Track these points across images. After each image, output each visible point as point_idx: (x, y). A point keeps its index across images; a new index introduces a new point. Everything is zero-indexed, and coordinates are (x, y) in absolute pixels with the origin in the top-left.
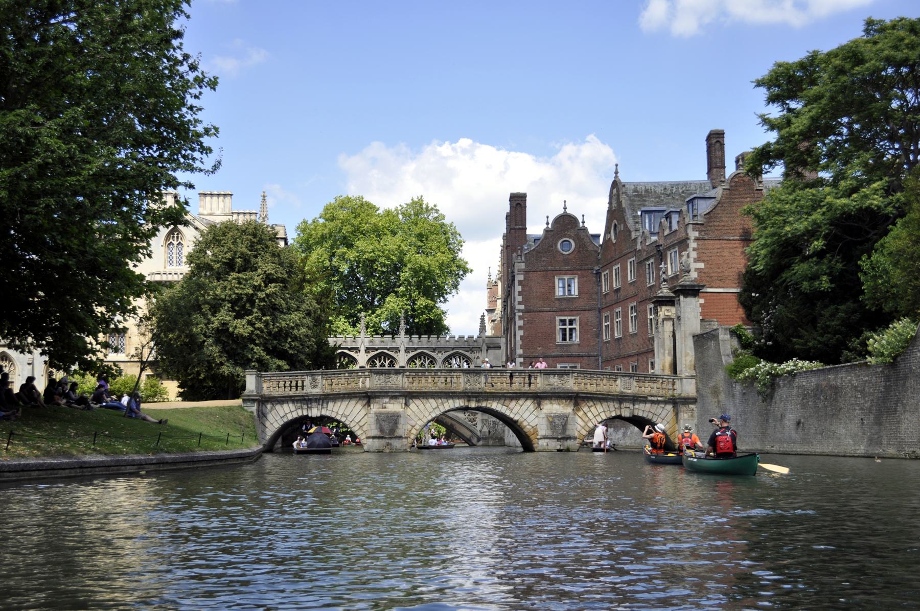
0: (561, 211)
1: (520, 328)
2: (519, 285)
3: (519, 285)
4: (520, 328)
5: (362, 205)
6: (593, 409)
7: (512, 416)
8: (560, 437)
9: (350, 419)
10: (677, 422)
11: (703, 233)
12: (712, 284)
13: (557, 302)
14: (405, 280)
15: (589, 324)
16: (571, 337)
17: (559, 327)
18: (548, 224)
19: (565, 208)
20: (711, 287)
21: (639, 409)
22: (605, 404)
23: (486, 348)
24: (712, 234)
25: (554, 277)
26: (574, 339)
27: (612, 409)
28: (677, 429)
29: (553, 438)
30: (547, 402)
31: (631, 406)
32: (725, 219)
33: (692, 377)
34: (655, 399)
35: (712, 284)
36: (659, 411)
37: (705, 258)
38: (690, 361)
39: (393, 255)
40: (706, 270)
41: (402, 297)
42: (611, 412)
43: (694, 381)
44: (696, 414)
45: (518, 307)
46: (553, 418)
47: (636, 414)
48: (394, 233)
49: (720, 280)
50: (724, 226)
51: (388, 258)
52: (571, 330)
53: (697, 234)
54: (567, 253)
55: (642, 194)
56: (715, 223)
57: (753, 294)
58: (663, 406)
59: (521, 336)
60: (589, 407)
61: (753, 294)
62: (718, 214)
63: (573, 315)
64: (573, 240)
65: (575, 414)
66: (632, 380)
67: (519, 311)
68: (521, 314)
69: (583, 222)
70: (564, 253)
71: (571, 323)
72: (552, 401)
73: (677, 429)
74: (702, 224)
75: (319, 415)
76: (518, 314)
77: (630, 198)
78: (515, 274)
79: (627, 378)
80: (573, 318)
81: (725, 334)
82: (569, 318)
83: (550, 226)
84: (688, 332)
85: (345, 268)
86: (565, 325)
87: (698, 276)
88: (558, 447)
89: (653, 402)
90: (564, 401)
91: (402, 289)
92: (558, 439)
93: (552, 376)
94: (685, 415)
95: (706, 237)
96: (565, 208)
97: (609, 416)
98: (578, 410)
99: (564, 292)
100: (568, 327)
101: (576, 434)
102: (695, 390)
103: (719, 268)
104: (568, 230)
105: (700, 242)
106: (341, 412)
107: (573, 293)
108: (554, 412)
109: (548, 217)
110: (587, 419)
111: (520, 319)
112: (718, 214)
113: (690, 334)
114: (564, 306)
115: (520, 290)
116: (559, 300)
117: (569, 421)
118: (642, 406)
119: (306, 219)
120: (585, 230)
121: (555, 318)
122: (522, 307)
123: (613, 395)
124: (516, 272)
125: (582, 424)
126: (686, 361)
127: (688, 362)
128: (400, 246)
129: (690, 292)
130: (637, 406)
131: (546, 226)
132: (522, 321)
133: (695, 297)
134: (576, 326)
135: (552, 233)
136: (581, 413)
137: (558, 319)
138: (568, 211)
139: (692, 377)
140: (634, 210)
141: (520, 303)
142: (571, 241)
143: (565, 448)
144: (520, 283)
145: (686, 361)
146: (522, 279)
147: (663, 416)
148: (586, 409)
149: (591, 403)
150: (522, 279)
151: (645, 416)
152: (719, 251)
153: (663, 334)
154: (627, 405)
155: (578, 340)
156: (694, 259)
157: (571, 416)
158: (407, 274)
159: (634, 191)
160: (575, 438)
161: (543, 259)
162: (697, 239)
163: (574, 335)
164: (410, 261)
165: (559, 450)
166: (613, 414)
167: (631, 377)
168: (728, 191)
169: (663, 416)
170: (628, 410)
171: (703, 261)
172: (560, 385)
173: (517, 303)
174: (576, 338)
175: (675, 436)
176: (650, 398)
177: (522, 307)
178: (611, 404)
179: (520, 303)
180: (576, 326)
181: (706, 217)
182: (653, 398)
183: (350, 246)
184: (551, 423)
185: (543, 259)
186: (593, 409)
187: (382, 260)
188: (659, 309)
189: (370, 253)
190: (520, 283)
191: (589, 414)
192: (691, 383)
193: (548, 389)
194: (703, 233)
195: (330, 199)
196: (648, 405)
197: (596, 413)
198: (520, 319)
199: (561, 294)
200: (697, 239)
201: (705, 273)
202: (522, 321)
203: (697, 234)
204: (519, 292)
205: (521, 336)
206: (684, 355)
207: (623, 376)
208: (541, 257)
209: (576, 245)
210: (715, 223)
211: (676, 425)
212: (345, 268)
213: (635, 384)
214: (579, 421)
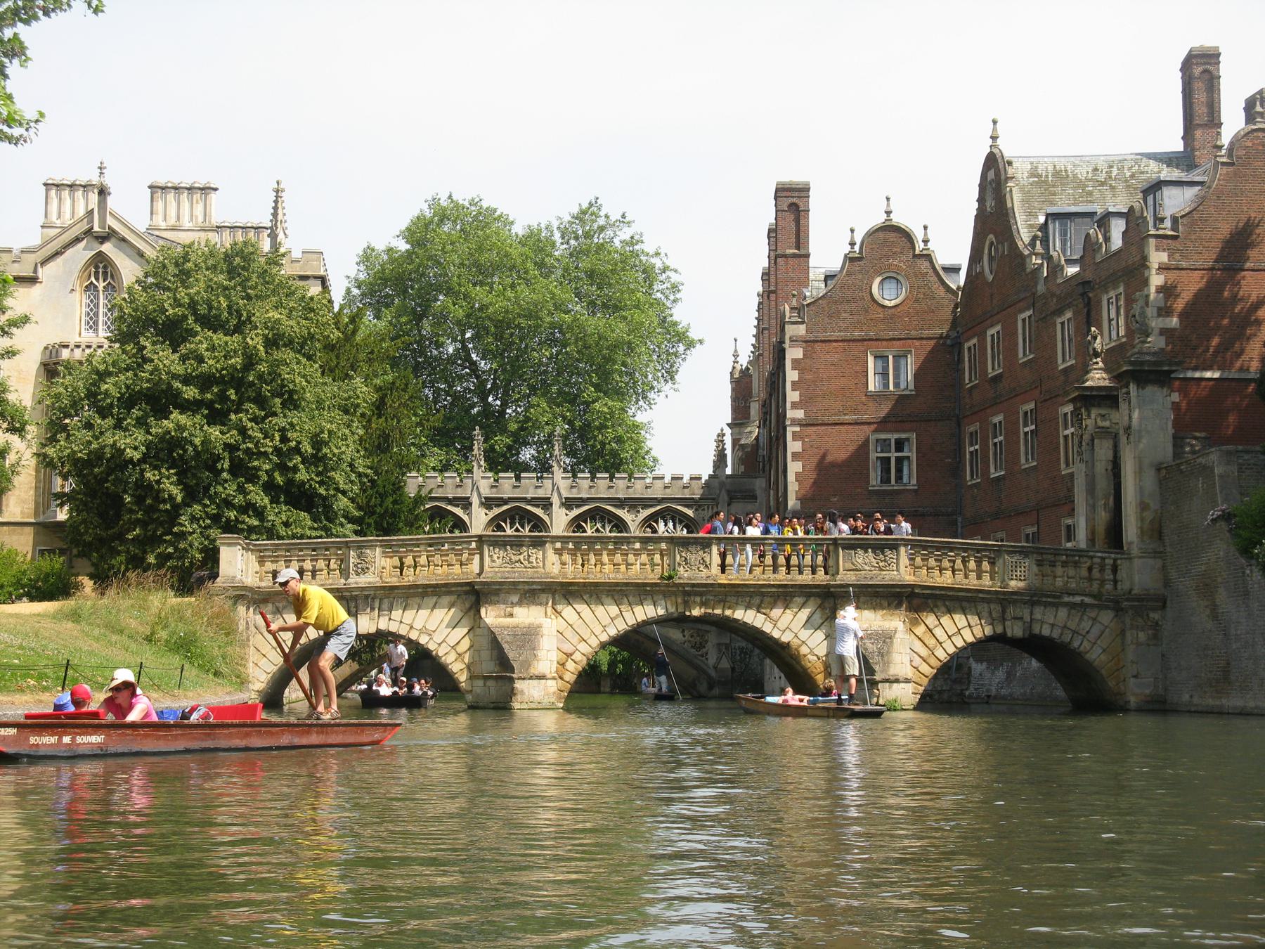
0: (880, 219)
1: (796, 456)
3: (794, 368)
4: (796, 456)
7: (776, 634)
9: (438, 638)
11: (1177, 256)
16: (899, 478)
18: (852, 244)
19: (888, 213)
23: (726, 498)
24: (1196, 257)
47: (1036, 630)
54: (893, 303)
59: (797, 474)
63: (904, 431)
67: (795, 422)
69: (926, 241)
70: (887, 303)
71: (900, 445)
75: (373, 630)
80: (904, 436)
82: (896, 436)
83: (857, 248)
95: (1184, 264)
96: (888, 213)
106: (418, 625)
109: (852, 231)
111: (794, 440)
120: (928, 257)
122: (799, 414)
124: (787, 341)
131: (848, 248)
134: (910, 452)
138: (897, 219)
147: (1092, 636)
155: (914, 481)
162: (1162, 268)
169: (1092, 636)
170: (1020, 623)
177: (799, 414)
179: (795, 406)
190: (796, 362)
191: (939, 632)
194: (1177, 256)
198: (794, 440)
204: (793, 383)
205: (797, 474)
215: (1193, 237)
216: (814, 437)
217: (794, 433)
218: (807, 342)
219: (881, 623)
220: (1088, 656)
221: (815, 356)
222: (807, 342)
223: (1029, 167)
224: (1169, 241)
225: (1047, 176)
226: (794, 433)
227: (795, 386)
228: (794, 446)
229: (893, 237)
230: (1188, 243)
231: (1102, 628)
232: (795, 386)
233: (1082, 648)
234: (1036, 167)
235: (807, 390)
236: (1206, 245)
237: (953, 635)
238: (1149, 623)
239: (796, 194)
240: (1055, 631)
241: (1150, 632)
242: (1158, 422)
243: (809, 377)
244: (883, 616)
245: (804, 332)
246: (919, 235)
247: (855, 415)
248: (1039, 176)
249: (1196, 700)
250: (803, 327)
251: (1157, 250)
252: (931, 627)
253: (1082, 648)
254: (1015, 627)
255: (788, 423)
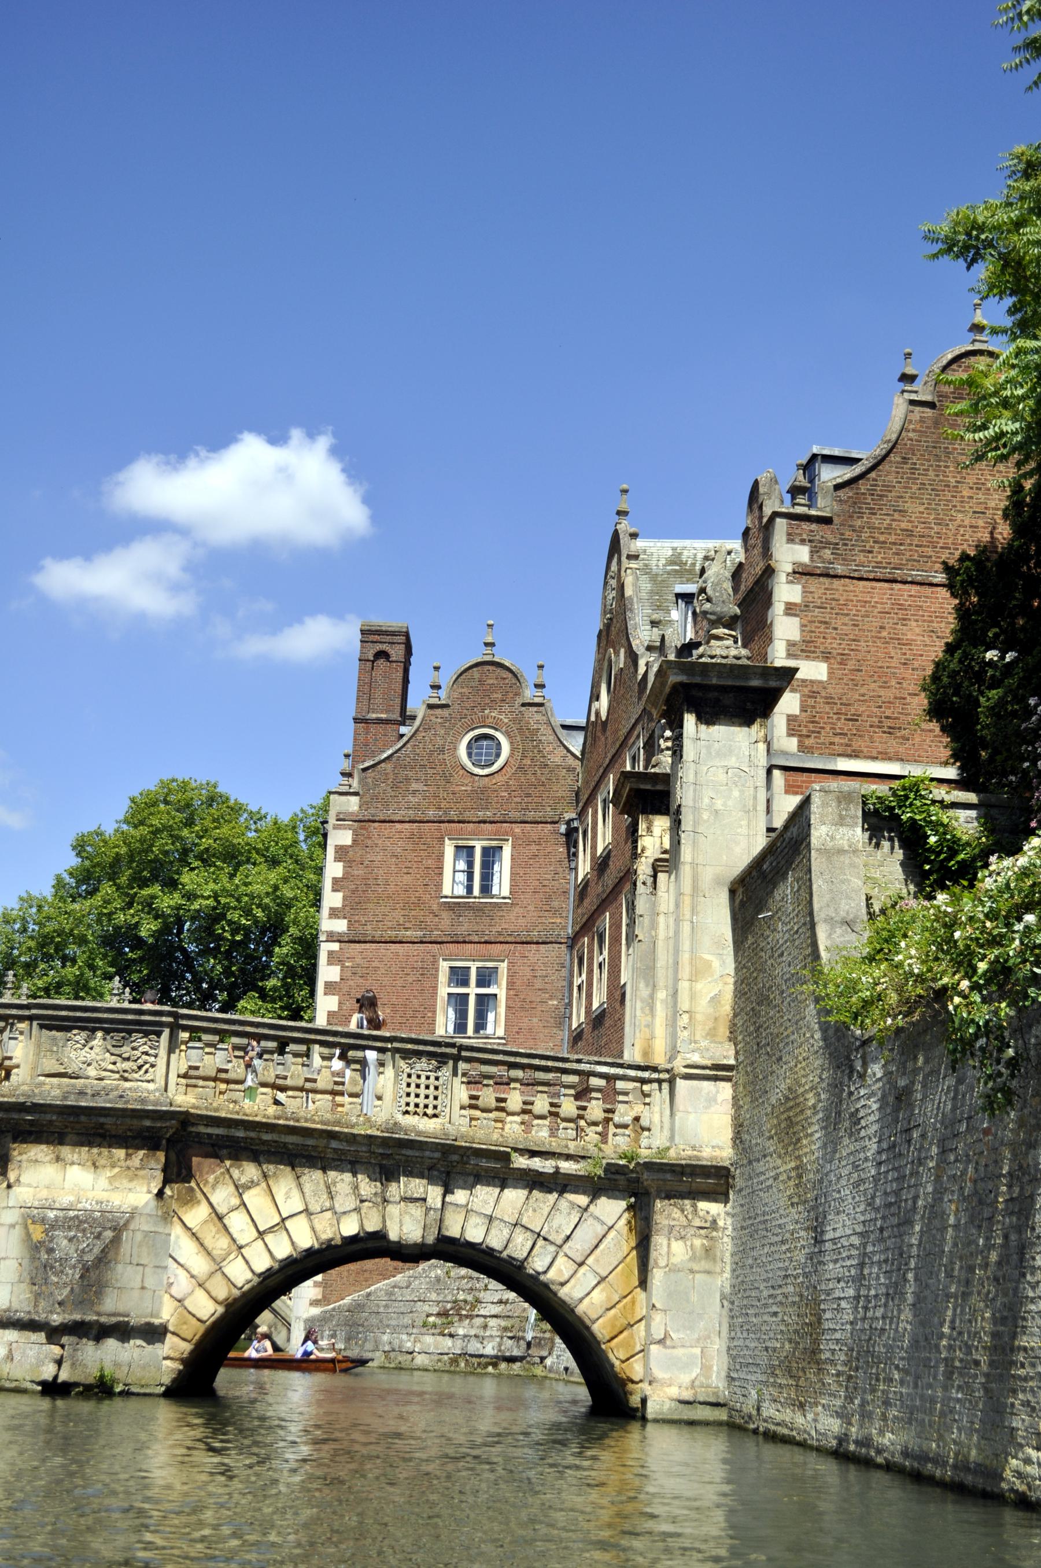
2: (337, 859)
3: (337, 859)
4: (330, 988)
5: (211, 800)
6: (255, 1198)
8: (56, 1319)
10: (643, 1283)
11: (827, 553)
12: (858, 744)
13: (445, 915)
14: (283, 963)
15: (538, 984)
16: (480, 1025)
17: (444, 989)
20: (855, 755)
21: (468, 1211)
22: (313, 1178)
24: (861, 557)
25: (441, 841)
26: (490, 1030)
27: (345, 1201)
28: (641, 1311)
29: (30, 1326)
30: (40, 1151)
31: (434, 1194)
32: (913, 508)
33: (718, 1072)
34: (545, 1166)
35: (858, 744)
36: (564, 1221)
37: (833, 645)
38: (715, 1000)
39: (259, 906)
40: (834, 691)
41: (273, 1000)
42: (339, 1216)
43: (725, 1091)
44: (726, 1245)
45: (328, 925)
46: (54, 1225)
47: (453, 1231)
48: (274, 862)
49: (890, 731)
50: (909, 533)
51: (248, 912)
52: (481, 999)
53: (803, 554)
55: (789, 729)
56: (876, 521)
57: (991, 655)
58: (582, 1200)
60: (240, 1189)
61: (991, 655)
62: (889, 488)
64: (507, 734)
65: (168, 1217)
66: (446, 1072)
67: (332, 937)
68: (335, 946)
71: (485, 978)
72: (66, 1151)
73: (641, 1311)
74: (827, 521)
76: (325, 948)
77: (654, 578)
78: (329, 827)
79: (422, 1065)
81: (841, 821)
82: (480, 964)
84: (707, 875)
85: (148, 928)
86: (465, 983)
87: (803, 709)
88: (48, 1372)
89: (535, 1182)
90: (120, 1153)
91: (272, 982)
92: (54, 1334)
93: (80, 1036)
94: (678, 1247)
95: (840, 569)
97: (327, 1233)
98: (189, 1200)
99: (469, 889)
100: (473, 991)
101: (166, 1313)
102: (728, 1134)
103: (885, 686)
104: (493, 704)
105: (814, 584)
107: (495, 891)
108: (65, 1200)
110: (224, 1242)
111: (330, 963)
112: (889, 488)
113: (717, 881)
114: (465, 926)
115: (339, 874)
116: (455, 908)
117: (125, 1248)
118: (484, 1196)
119: (103, 828)
121: (435, 962)
122: (340, 926)
123: (353, 1138)
124: (332, 821)
125: (200, 1265)
126: (693, 996)
127: (703, 1005)
128: (276, 888)
129: (728, 700)
130: (460, 1196)
132: (338, 968)
133: (748, 723)
134: (499, 990)
135: (445, 712)
136: (196, 1215)
137: (444, 966)
139: (718, 1072)
140: (659, 608)
141: (334, 913)
142: (498, 735)
143: (88, 1374)
144: (341, 853)
145: (693, 996)
146: (348, 841)
147: (577, 1247)
148: (222, 1196)
149: (250, 1171)
150: (348, 841)
151: (495, 1242)
152: (888, 622)
153: (654, 925)
154: (416, 1186)
155: (500, 1032)
156: (791, 644)
157: (143, 1225)
158: (285, 950)
159: (671, 562)
160: (154, 1333)
161: (414, 786)
162: (801, 573)
163: (491, 1016)
164: (295, 922)
165: (52, 1389)
166: (350, 1228)
167: (442, 1059)
168: (928, 412)
169: (577, 1247)
170: (416, 1211)
171: (826, 657)
172: (111, 1081)
173: (325, 912)
174: (496, 1026)
175: (628, 1344)
176: (521, 1162)
177: (340, 926)
178: (342, 1181)
179: (334, 913)
180: (499, 990)
181: (844, 494)
182: (537, 1164)
183: (172, 884)
184: (34, 1248)
185: (414, 786)
186: (255, 1198)
187: (234, 916)
188: (642, 826)
189: (208, 898)
190: (341, 853)
191: (238, 1222)
192: (711, 1100)
193: (53, 1091)
194: (827, 553)
195: (148, 783)
196: (514, 1196)
197: (267, 1219)
198: (330, 963)
199: (461, 890)
200: (801, 573)
201: (829, 700)
202: (338, 968)
203: (803, 554)
204: (335, 881)
206: (685, 972)
207: (406, 1054)
208: (407, 780)
209: (513, 750)
210: (876, 521)
211: (640, 1295)
212: (148, 928)
213: (461, 1093)
214: (185, 1249)
215: (858, 523)
216: (358, 960)
217: (330, 953)
218: (361, 823)
219: (104, 1196)
220: (563, 1293)
221: (369, 842)
222: (361, 823)
223: (670, 553)
224: (814, 526)
225: (694, 565)
226: (330, 953)
227: (337, 884)
228: (327, 973)
229: (492, 677)
230: (848, 534)
231: (600, 1230)
232: (337, 884)
233: (551, 1275)
234: (680, 554)
235: (353, 892)
236: (882, 538)
237: (271, 1230)
238: (697, 1223)
239: (388, 638)
240: (493, 1232)
241: (698, 1242)
242: (736, 793)
243: (358, 872)
244: (111, 1179)
245: (356, 808)
246: (530, 676)
247: (421, 929)
248: (682, 564)
249: (769, 1410)
250: (354, 800)
251: (790, 540)
252: (222, 1210)
253: (551, 1275)
254: (407, 1219)
255: (322, 937)
